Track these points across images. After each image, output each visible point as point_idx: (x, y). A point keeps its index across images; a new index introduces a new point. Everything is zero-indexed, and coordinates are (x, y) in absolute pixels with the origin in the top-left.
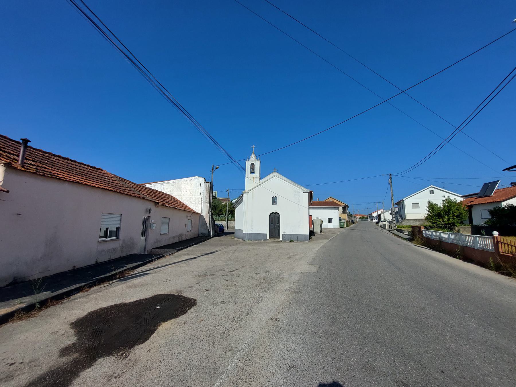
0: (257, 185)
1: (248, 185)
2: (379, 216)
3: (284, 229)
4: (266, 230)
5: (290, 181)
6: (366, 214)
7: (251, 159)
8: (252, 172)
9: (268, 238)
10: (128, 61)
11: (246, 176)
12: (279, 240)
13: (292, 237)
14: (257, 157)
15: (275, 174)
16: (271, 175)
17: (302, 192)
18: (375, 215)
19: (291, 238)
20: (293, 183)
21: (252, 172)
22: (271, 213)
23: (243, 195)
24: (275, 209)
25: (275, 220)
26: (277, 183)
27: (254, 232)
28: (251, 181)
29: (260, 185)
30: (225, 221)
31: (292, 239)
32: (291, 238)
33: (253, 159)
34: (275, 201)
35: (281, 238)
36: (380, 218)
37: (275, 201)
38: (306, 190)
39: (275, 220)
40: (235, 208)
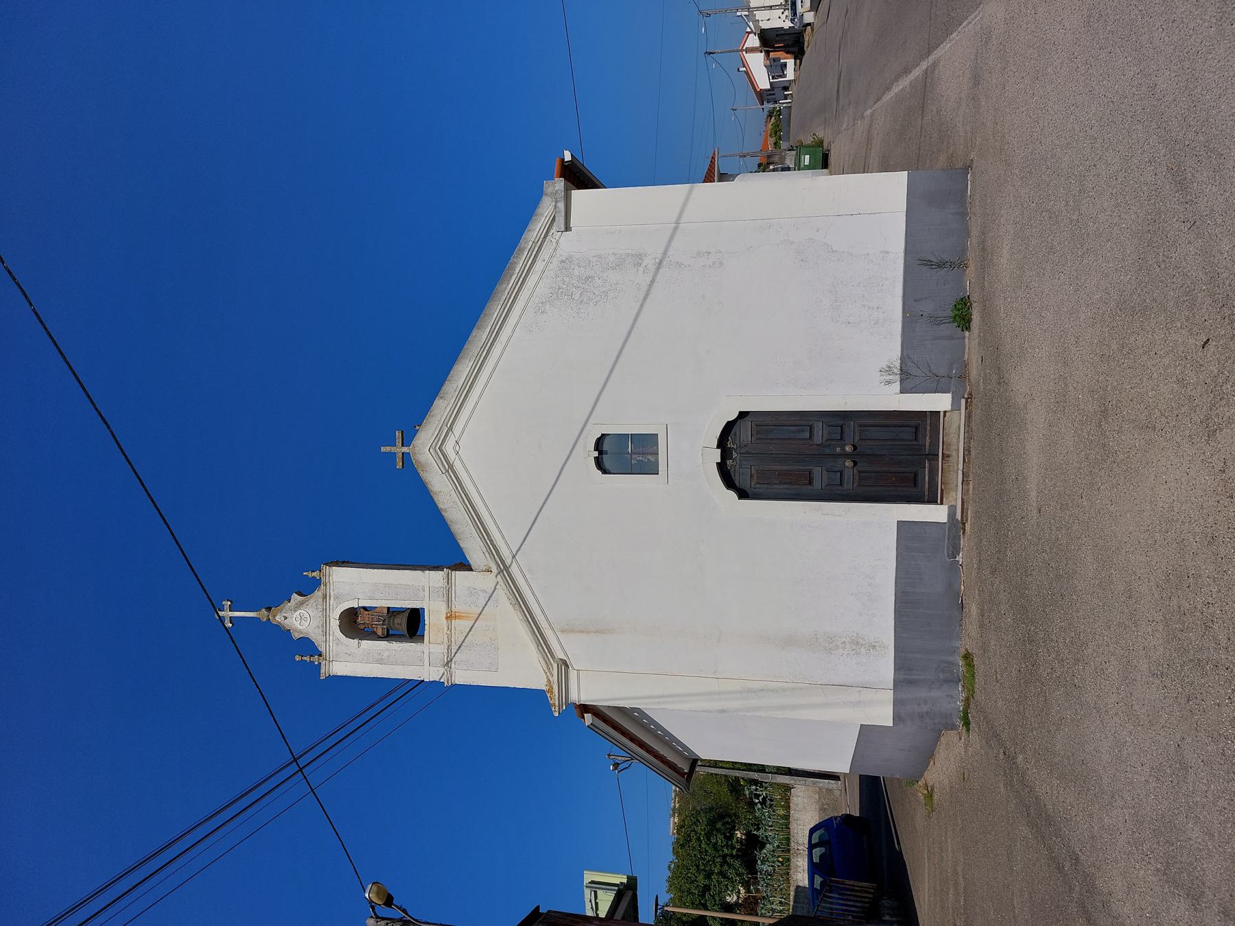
0: (502, 594)
1: (512, 665)
2: (769, 40)
3: (864, 379)
4: (862, 539)
5: (480, 336)
6: (760, 112)
7: (316, 636)
8: (411, 624)
9: (936, 514)
10: (606, 736)
11: (431, 673)
12: (955, 434)
13: (928, 307)
14: (308, 588)
15: (423, 447)
16: (438, 483)
17: (565, 244)
18: (757, 64)
19: (935, 320)
20: (495, 311)
21: (411, 624)
22: (729, 482)
23: (584, 709)
24: (692, 454)
25: (775, 456)
26: (489, 437)
27: (884, 628)
28: (476, 641)
29: (504, 569)
30: (788, 788)
31: (945, 302)
32: (935, 320)
33: (300, 618)
34: (624, 454)
35: (940, 402)
36: (779, 32)
37: (624, 454)
38: (547, 207)
39: (775, 456)
40: (694, 762)
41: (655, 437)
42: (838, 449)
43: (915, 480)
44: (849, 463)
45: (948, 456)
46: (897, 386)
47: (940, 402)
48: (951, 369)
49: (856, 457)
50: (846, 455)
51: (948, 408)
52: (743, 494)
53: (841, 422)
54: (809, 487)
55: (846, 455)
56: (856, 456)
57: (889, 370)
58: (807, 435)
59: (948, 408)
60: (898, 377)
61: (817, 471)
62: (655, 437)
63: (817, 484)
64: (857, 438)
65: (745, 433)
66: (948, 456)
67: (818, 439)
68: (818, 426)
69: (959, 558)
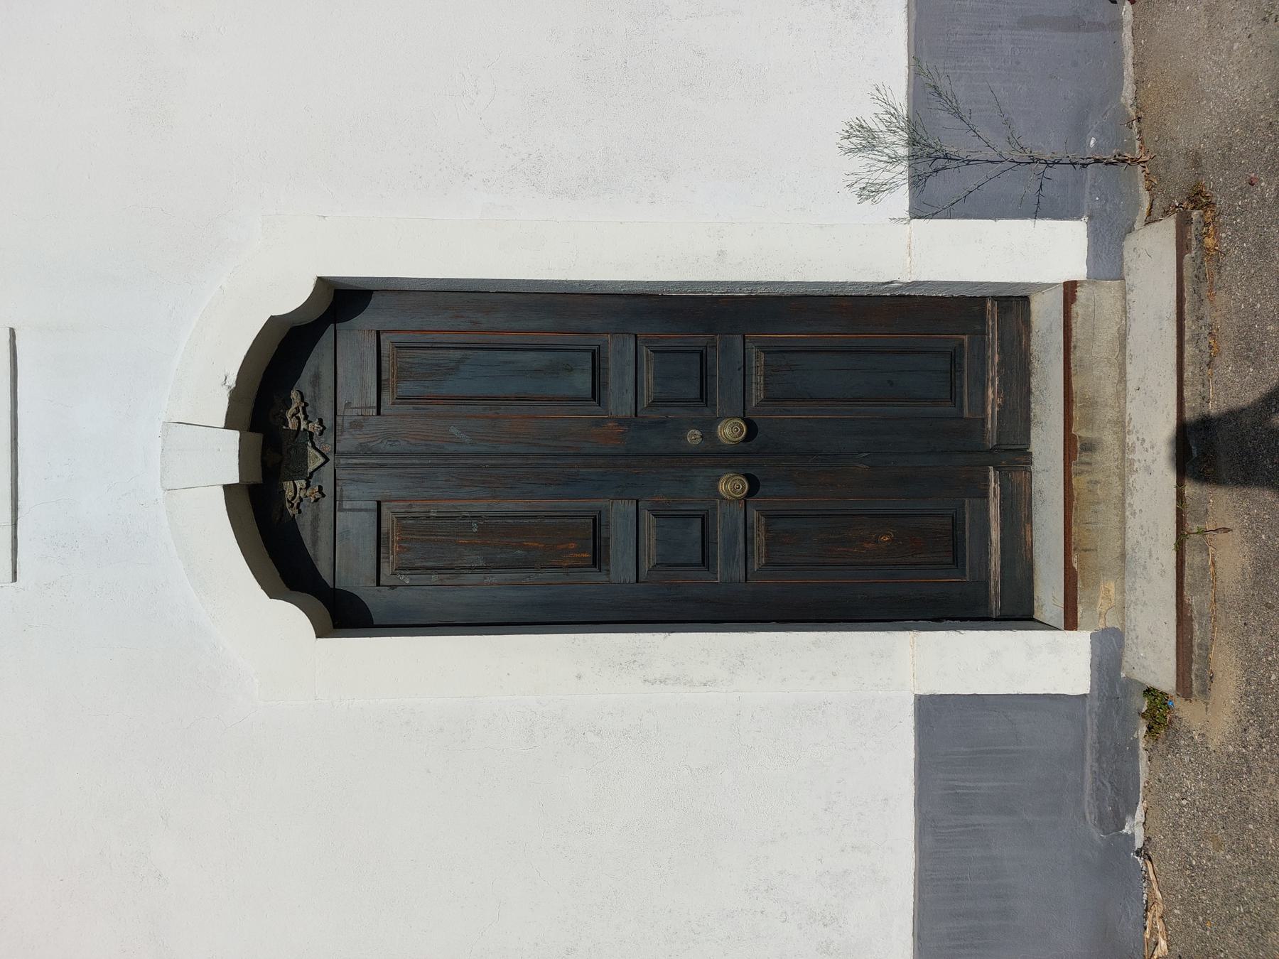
9: (1042, 663)
35: (1033, 252)
41: (318, 636)
42: (693, 437)
43: (953, 542)
44: (730, 486)
45: (1090, 447)
46: (900, 199)
47: (1033, 252)
48: (1080, 132)
49: (752, 456)
50: (722, 458)
51: (1077, 269)
52: (342, 614)
53: (701, 340)
54: (594, 576)
55: (722, 458)
56: (752, 456)
57: (864, 139)
58: (582, 382)
59: (1077, 269)
60: (901, 173)
61: (619, 514)
62: (318, 636)
63: (621, 566)
64: (757, 393)
65: (347, 366)
66: (1090, 447)
67: (620, 401)
68: (620, 354)
69: (1135, 828)
